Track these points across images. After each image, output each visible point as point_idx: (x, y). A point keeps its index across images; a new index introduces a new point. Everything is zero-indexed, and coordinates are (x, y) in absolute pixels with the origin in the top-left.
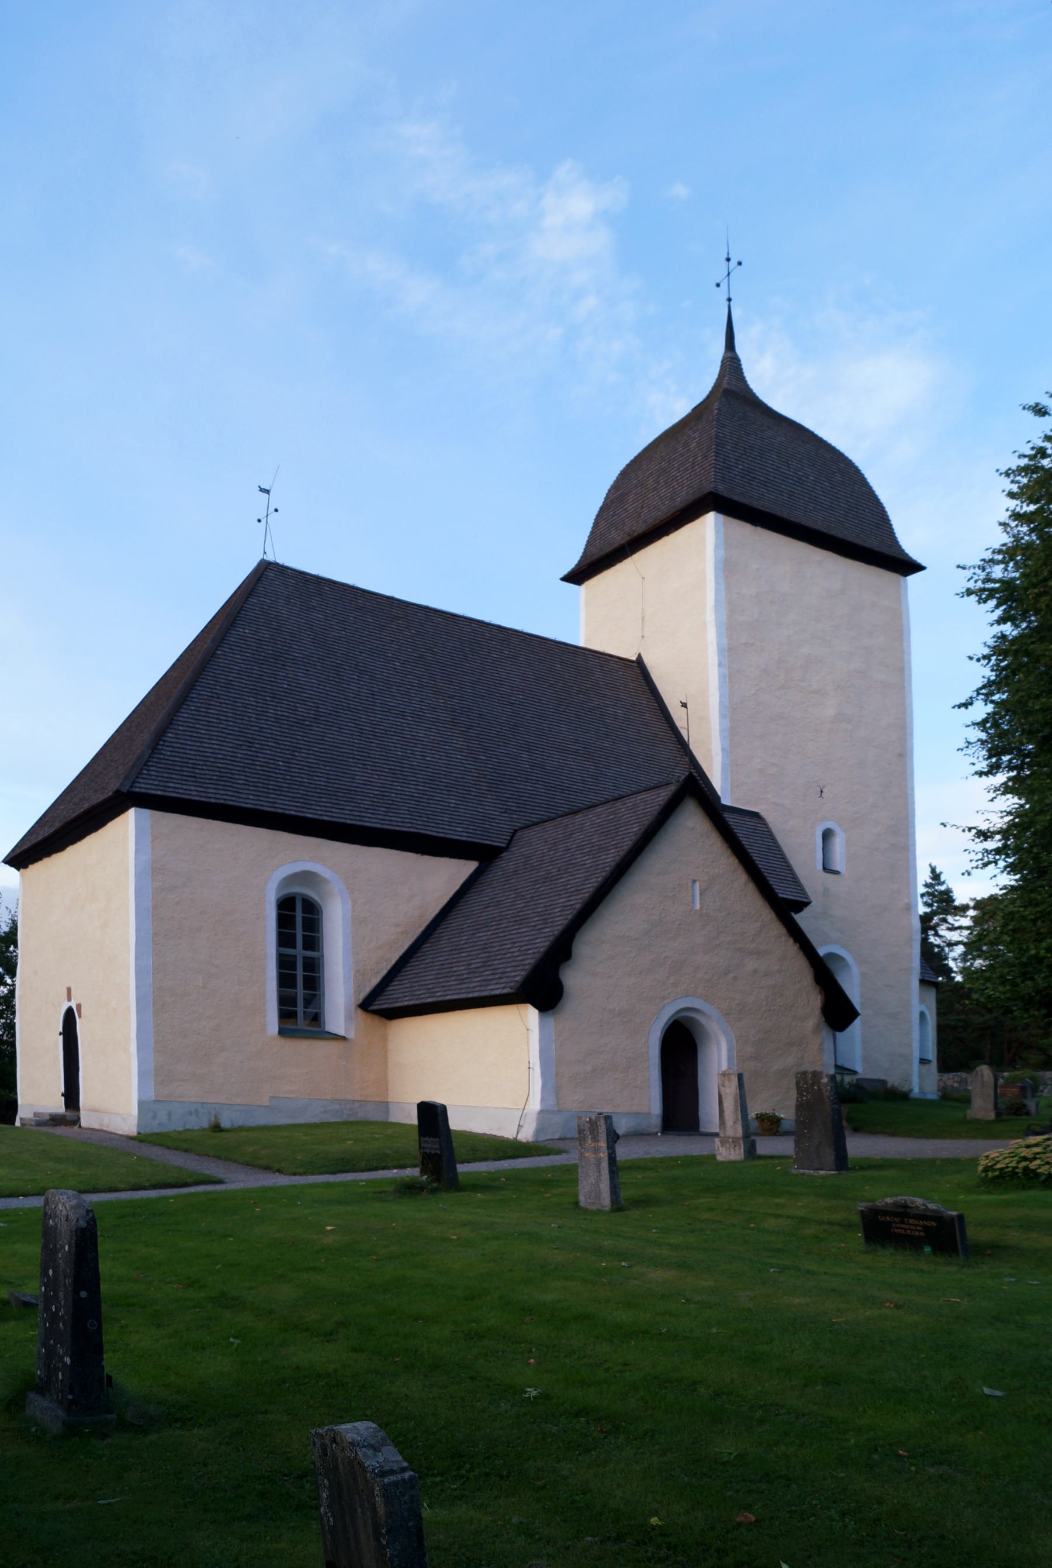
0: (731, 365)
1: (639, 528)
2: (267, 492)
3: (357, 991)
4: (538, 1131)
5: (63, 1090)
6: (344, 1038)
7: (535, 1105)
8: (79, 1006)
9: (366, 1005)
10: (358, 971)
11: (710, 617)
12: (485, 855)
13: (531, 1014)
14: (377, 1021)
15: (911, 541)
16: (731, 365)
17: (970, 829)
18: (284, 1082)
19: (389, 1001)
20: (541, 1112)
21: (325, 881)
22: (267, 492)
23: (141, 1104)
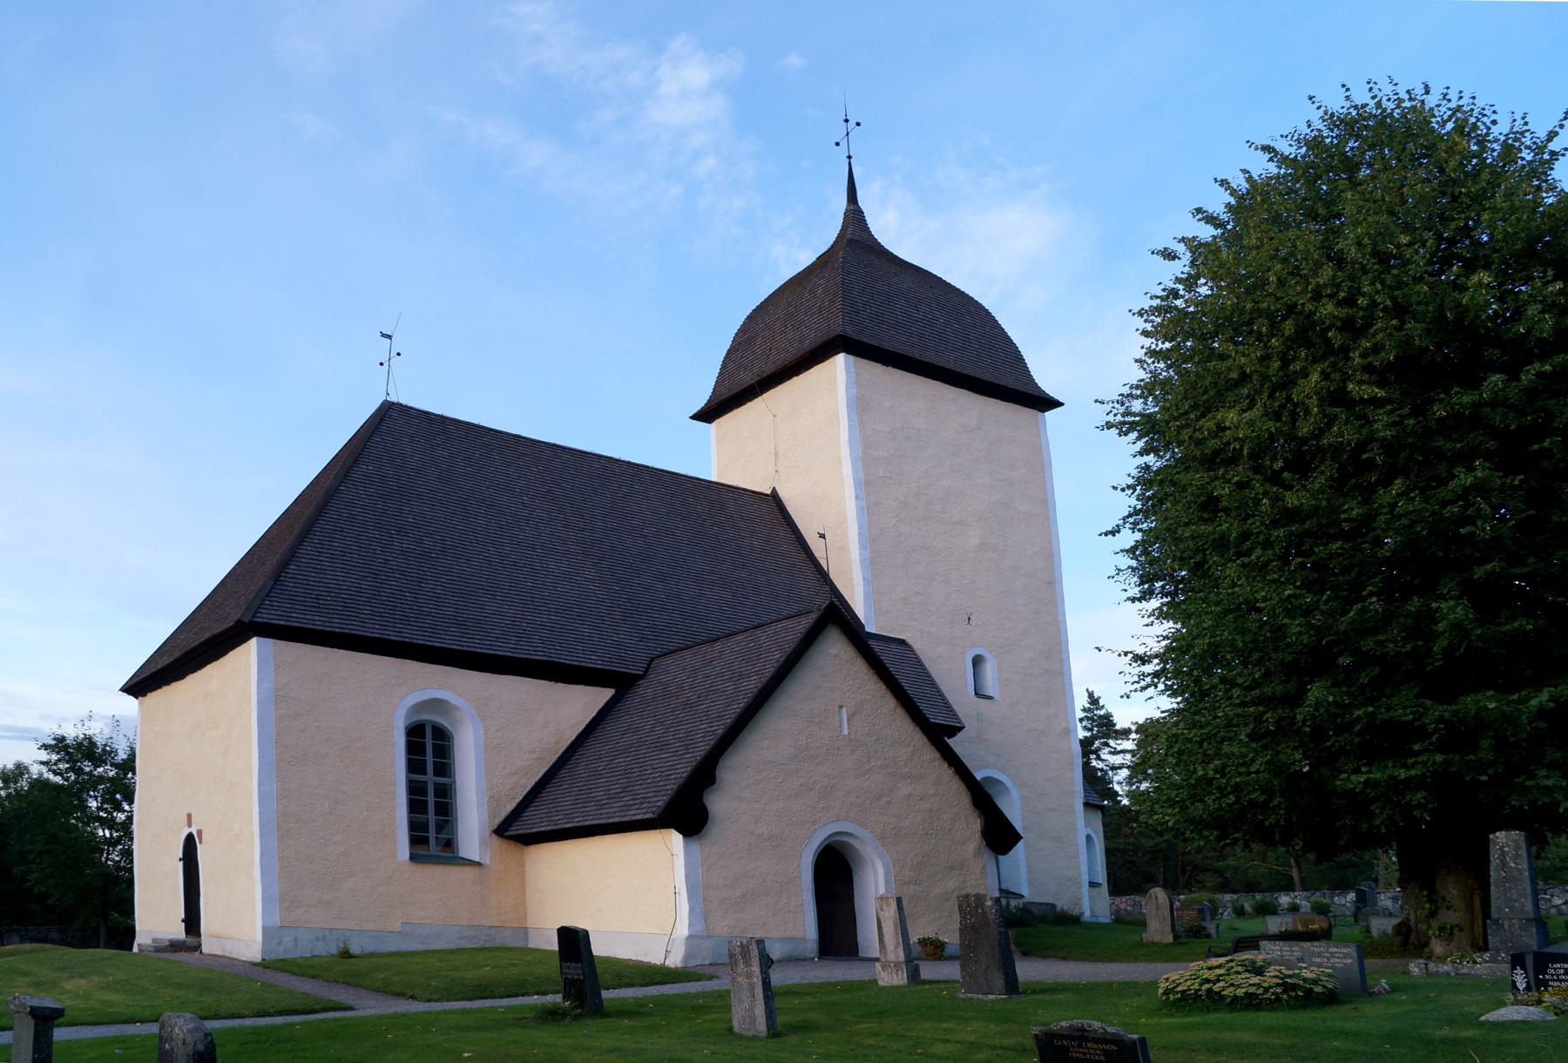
0: (855, 216)
1: (769, 369)
2: (390, 337)
3: (492, 815)
4: (687, 957)
6: (479, 864)
7: (683, 930)
8: (200, 832)
9: (501, 831)
10: (491, 797)
11: (845, 452)
12: (622, 683)
13: (675, 839)
14: (513, 847)
15: (1046, 379)
16: (855, 216)
17: (1126, 654)
19: (523, 827)
20: (689, 937)
21: (456, 708)
22: (390, 337)
23: (265, 930)
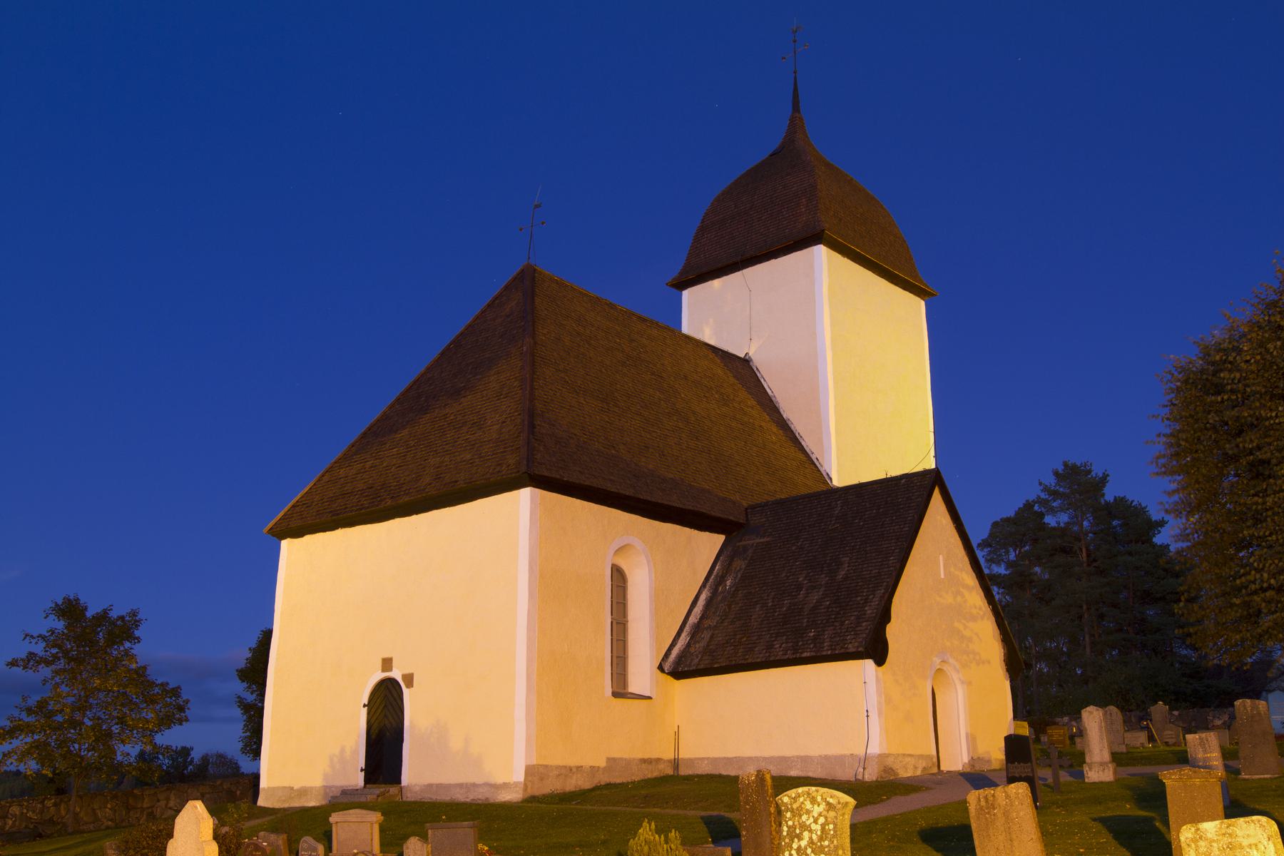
0: (795, 125)
5: (362, 764)
6: (650, 698)
8: (409, 679)
16: (795, 125)
18: (610, 741)
19: (682, 667)
